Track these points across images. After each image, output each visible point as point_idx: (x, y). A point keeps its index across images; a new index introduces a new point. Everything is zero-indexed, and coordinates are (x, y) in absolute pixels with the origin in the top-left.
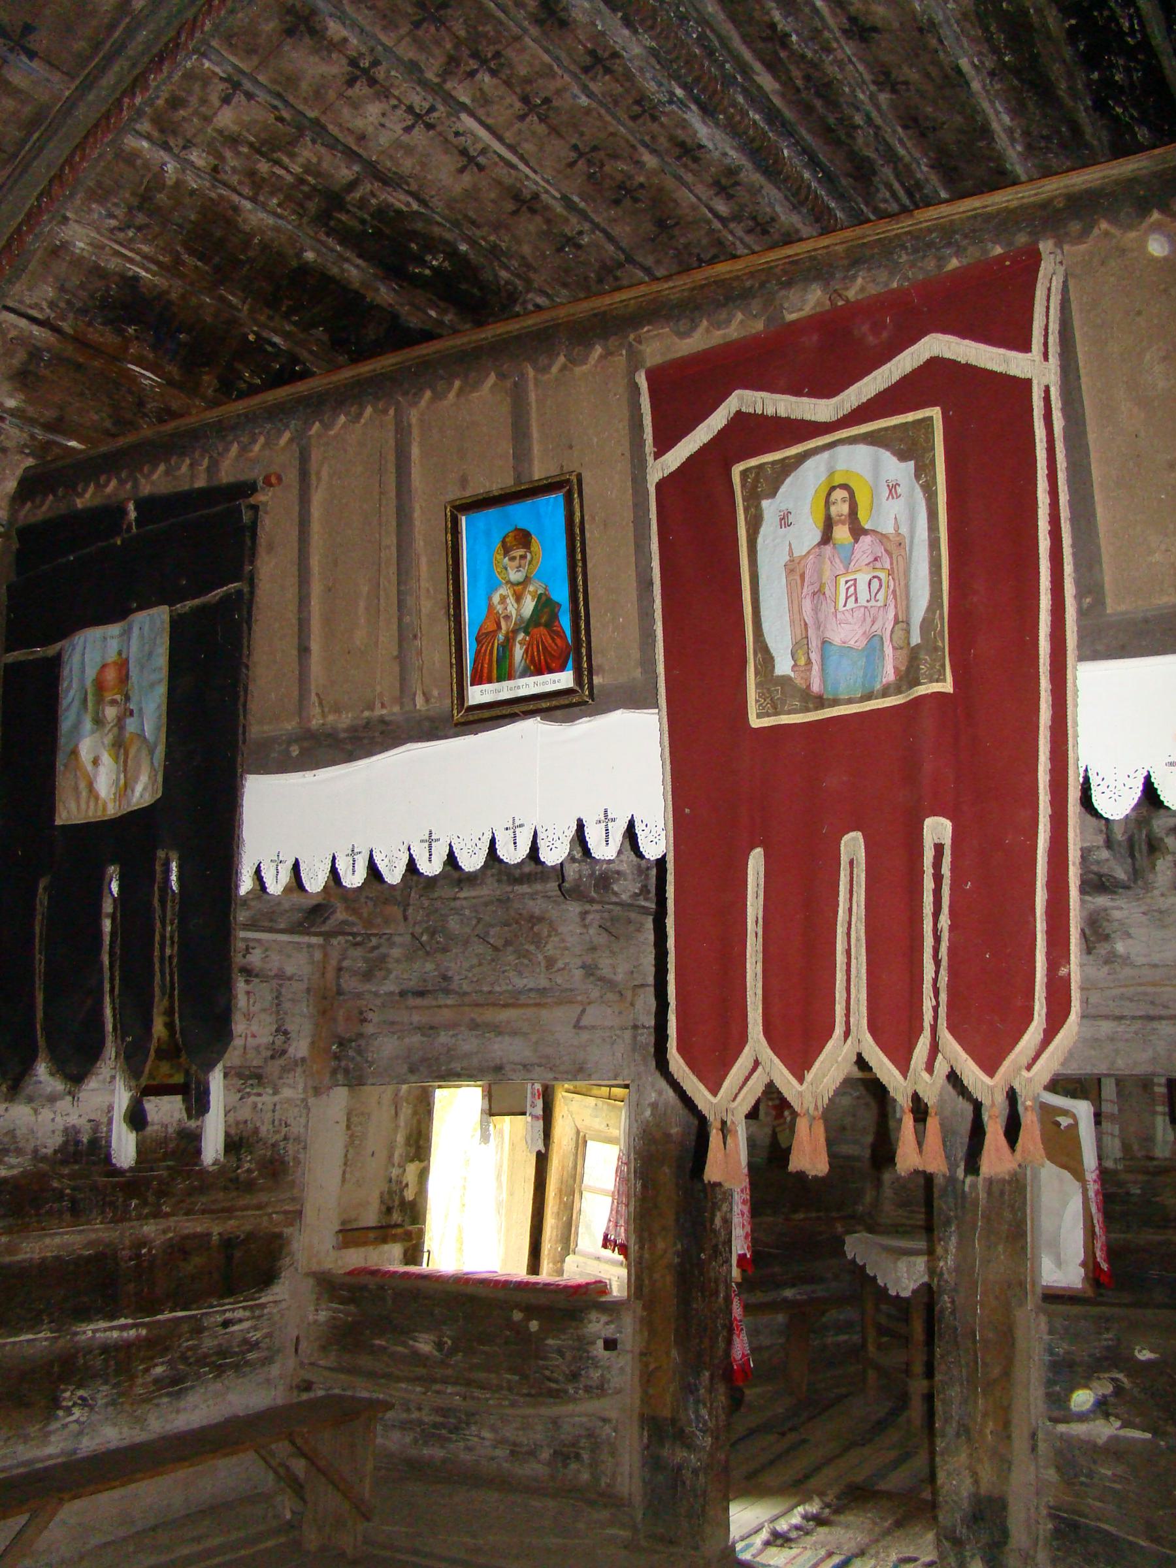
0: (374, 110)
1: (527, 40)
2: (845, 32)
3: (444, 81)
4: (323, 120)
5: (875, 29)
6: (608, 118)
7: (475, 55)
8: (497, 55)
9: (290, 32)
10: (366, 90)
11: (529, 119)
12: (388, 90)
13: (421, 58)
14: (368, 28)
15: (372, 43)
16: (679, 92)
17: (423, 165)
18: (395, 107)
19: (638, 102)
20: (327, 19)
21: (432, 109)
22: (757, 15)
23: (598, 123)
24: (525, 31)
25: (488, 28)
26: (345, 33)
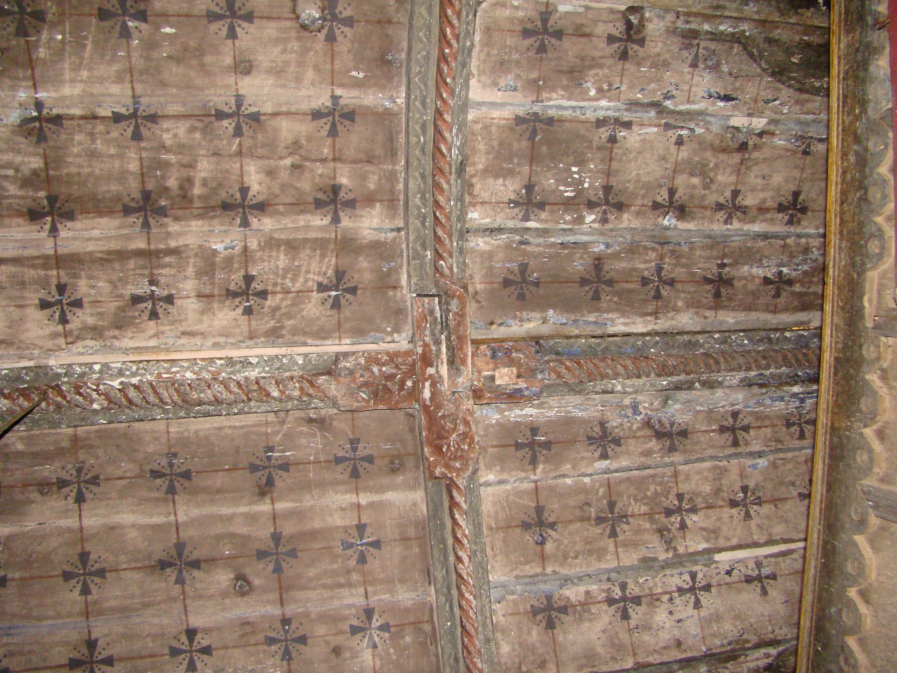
0: (661, 616)
1: (681, 467)
2: (790, 222)
3: (675, 549)
4: (641, 659)
5: (796, 194)
6: (790, 455)
7: (669, 512)
8: (680, 497)
9: (550, 625)
10: (641, 609)
11: (752, 513)
12: (652, 595)
13: (643, 552)
14: (590, 570)
15: (604, 577)
16: (796, 389)
17: (738, 617)
18: (671, 599)
19: (789, 425)
20: (561, 592)
21: (693, 576)
22: (751, 287)
23: (789, 466)
24: (672, 464)
25: (652, 488)
26: (582, 589)
